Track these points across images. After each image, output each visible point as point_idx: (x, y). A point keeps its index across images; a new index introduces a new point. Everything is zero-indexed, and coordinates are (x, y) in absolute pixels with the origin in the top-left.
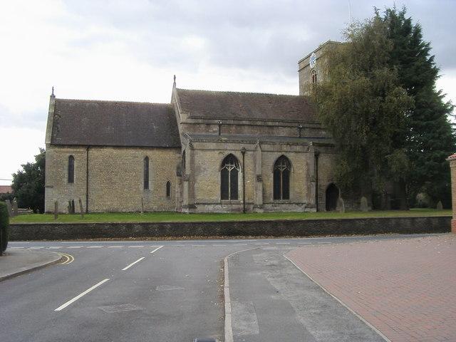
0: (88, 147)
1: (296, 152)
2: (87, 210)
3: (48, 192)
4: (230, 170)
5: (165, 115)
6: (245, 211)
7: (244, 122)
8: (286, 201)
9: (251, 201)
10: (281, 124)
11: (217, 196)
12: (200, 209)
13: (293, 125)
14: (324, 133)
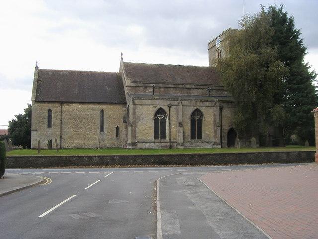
0: (62, 103)
1: (206, 106)
2: (61, 147)
3: (34, 134)
4: (160, 119)
5: (115, 80)
6: (171, 147)
7: (170, 85)
8: (199, 140)
9: (175, 141)
10: (196, 86)
11: (151, 137)
12: (139, 146)
13: (205, 87)
14: (226, 93)
